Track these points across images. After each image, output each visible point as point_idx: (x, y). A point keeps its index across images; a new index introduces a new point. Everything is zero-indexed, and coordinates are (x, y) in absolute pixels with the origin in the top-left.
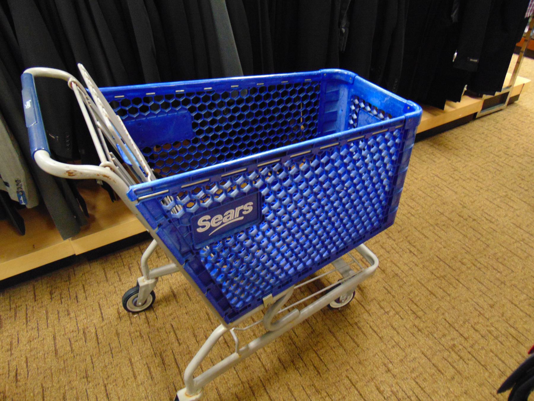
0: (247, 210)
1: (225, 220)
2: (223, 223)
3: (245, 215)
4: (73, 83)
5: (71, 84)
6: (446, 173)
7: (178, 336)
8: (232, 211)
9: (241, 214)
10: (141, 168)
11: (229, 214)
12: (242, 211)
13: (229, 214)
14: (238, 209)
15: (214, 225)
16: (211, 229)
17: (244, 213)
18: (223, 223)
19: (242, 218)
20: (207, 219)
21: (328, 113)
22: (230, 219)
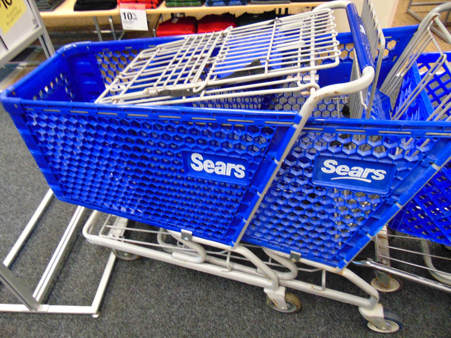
2: (347, 175)
13: (357, 170)
16: (335, 175)
18: (347, 175)
19: (369, 181)
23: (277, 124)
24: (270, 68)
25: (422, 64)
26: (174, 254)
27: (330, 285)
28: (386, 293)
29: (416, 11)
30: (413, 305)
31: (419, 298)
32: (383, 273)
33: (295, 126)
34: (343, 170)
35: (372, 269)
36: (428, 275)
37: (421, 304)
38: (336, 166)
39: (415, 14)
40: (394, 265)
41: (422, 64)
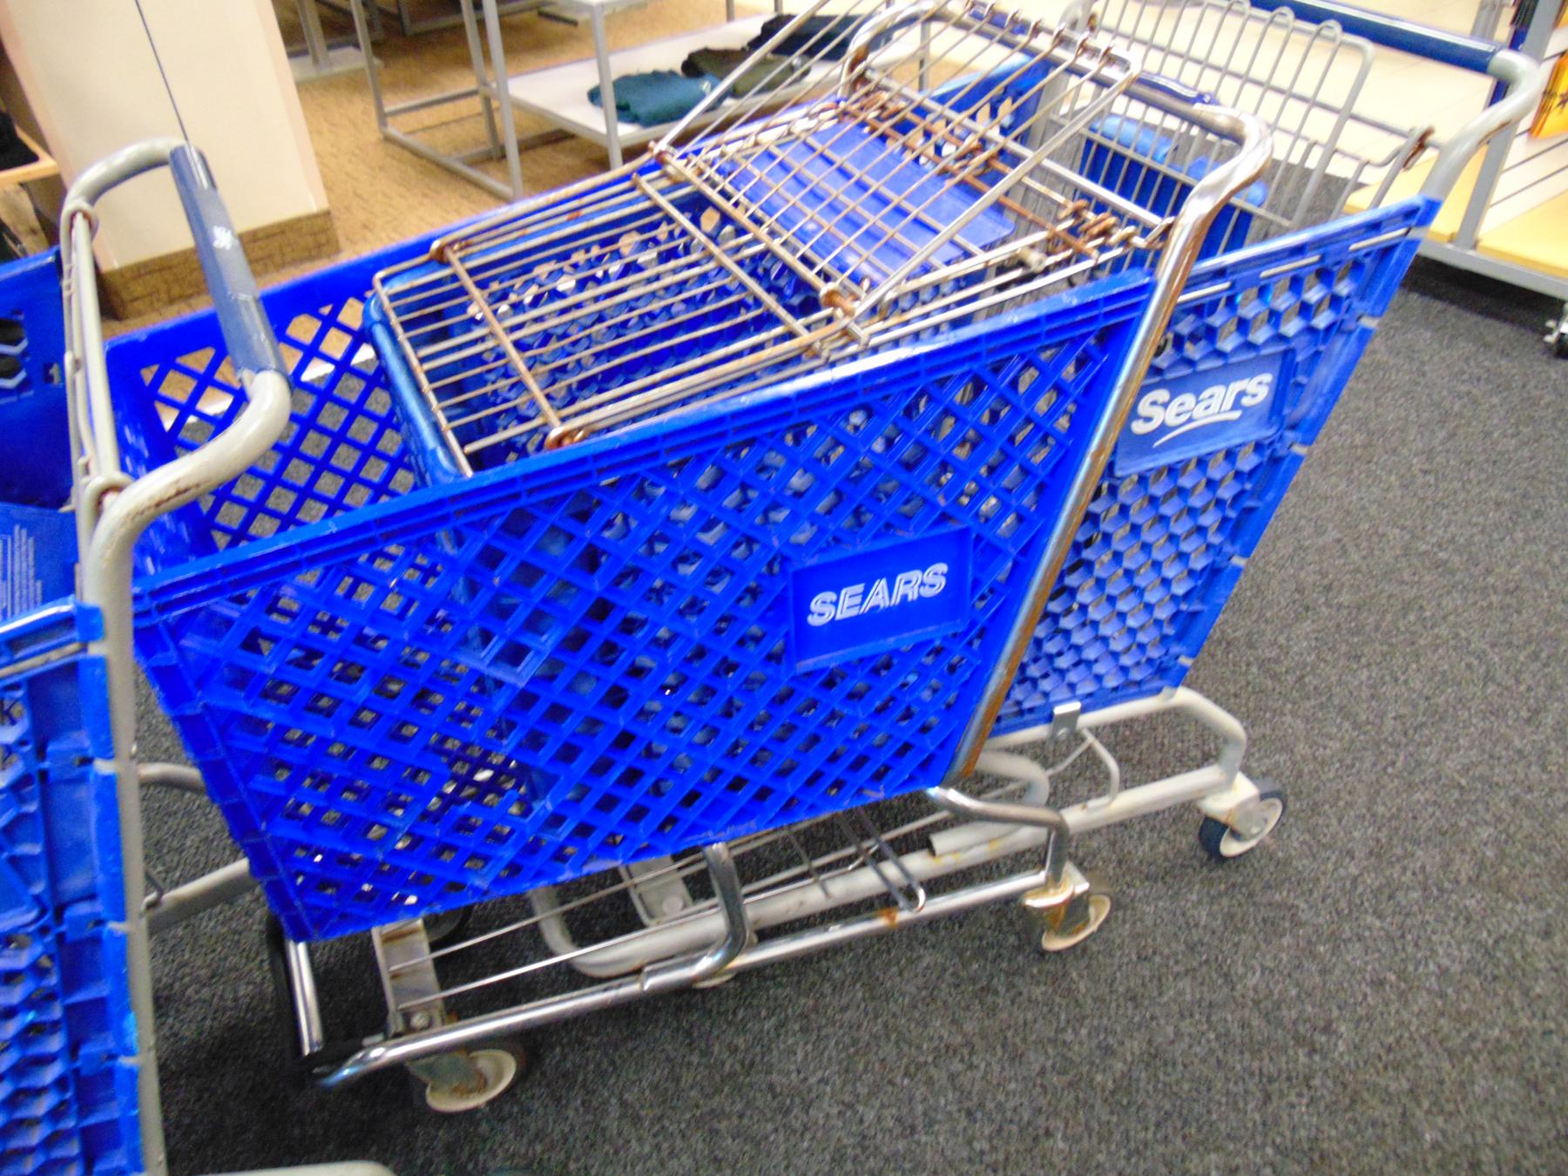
0: (1254, 396)
1: (1199, 412)
2: (1190, 420)
3: (1245, 409)
4: (79, 217)
5: (73, 216)
6: (1346, 717)
7: (1337, 410)
8: (1218, 390)
9: (1236, 405)
10: (1148, 127)
11: (1211, 397)
12: (1241, 394)
13: (1211, 397)
14: (1236, 387)
15: (1172, 420)
16: (1163, 429)
17: (1246, 401)
18: (1190, 420)
19: (1236, 415)
20: (1161, 400)
21: (352, 1085)
22: (1210, 411)
23: (20, 673)
24: (784, 244)
25: (155, 368)
26: (941, 841)
27: (1139, 771)
28: (491, 1103)
29: (409, 129)
30: (584, 1085)
31: (597, 1048)
32: (432, 1059)
33: (95, 650)
34: (1182, 409)
35: (396, 1070)
36: (571, 978)
37: (605, 1065)
38: (1165, 405)
39: (409, 140)
40: (459, 1010)
41: (155, 368)
